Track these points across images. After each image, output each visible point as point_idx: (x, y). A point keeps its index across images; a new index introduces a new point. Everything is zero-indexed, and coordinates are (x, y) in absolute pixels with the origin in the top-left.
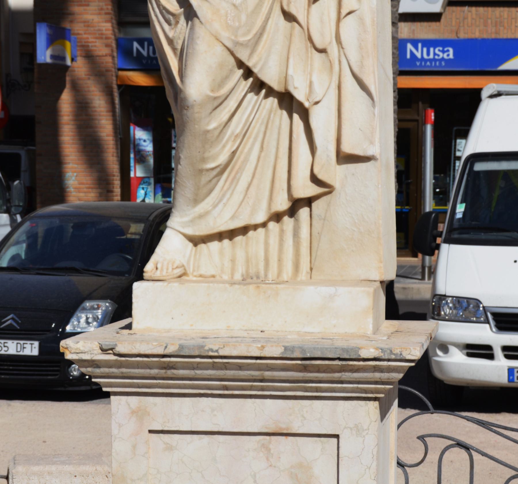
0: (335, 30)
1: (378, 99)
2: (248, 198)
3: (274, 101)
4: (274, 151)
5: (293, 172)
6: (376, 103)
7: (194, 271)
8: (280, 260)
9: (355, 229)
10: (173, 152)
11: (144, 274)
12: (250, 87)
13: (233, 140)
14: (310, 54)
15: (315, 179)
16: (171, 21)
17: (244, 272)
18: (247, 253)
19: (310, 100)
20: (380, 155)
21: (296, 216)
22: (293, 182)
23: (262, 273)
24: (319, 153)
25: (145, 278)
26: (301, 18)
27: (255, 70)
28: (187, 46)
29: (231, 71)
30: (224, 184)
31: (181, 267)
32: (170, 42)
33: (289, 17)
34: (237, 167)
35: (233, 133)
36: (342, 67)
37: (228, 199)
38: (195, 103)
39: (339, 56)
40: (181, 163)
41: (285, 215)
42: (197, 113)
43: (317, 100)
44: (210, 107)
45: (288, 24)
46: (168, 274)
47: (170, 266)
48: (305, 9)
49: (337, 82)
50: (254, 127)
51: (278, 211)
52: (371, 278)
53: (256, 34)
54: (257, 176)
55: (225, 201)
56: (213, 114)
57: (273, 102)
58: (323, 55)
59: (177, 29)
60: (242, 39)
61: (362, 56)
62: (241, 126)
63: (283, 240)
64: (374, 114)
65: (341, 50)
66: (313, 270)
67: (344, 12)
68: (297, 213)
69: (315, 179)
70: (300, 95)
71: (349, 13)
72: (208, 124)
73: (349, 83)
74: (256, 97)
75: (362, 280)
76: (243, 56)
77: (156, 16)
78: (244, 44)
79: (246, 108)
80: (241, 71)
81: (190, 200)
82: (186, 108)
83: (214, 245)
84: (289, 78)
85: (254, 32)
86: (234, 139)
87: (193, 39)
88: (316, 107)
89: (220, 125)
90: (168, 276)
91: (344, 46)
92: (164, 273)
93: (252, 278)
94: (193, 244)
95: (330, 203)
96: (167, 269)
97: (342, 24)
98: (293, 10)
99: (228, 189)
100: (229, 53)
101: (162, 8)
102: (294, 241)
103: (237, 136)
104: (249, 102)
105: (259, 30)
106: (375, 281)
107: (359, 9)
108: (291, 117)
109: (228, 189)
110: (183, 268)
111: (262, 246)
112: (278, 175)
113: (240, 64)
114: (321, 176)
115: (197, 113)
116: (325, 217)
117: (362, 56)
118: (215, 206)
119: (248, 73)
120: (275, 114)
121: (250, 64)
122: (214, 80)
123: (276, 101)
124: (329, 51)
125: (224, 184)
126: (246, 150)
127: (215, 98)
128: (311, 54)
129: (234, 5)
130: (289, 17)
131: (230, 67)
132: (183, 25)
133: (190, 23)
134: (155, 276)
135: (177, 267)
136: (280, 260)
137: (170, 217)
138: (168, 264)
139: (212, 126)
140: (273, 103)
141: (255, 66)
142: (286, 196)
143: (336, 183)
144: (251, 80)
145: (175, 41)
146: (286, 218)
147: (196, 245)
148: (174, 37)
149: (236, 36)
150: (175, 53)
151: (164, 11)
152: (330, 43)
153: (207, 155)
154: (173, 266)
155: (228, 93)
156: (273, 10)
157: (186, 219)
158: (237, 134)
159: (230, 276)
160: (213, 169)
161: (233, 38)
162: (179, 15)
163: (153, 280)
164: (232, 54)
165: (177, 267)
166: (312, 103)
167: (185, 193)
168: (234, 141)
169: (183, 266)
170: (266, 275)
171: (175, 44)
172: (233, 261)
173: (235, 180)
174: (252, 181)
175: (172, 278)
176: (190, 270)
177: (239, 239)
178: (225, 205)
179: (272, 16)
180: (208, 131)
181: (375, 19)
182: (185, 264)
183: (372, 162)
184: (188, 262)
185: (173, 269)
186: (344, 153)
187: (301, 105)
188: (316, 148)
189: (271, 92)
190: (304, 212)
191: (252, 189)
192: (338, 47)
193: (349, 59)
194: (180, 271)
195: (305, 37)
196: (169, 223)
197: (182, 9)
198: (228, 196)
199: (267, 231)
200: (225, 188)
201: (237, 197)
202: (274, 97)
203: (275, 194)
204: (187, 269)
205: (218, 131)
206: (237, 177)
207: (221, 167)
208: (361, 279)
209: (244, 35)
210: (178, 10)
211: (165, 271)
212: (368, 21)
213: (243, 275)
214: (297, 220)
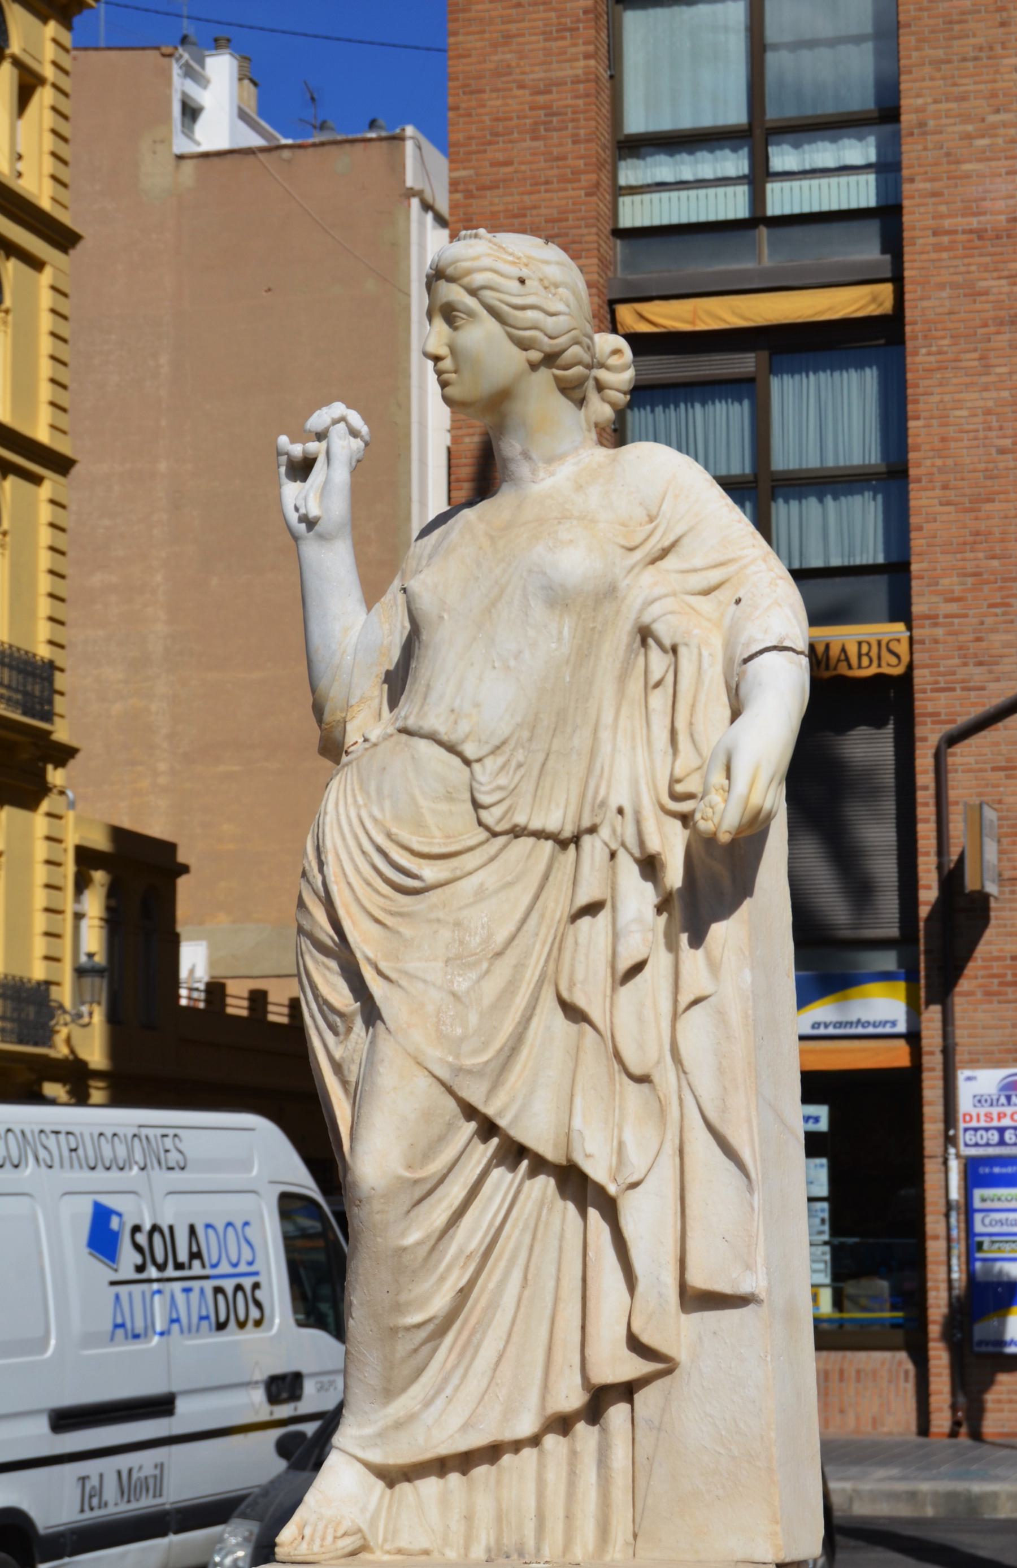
0: (669, 1035)
1: (760, 1176)
2: (497, 1384)
3: (548, 1182)
4: (551, 1284)
5: (589, 1329)
6: (754, 1183)
7: (385, 1540)
8: (569, 1517)
9: (722, 1451)
10: (823, 1191)
11: (277, 1550)
12: (494, 1155)
13: (462, 1264)
14: (618, 1086)
15: (636, 1345)
16: (337, 1027)
17: (492, 1543)
18: (498, 1501)
19: (620, 1181)
20: (769, 1291)
21: (602, 1421)
22: (588, 1351)
23: (531, 1543)
24: (641, 1287)
25: (278, 1557)
26: (595, 1014)
27: (502, 1123)
28: (364, 1078)
29: (450, 1126)
30: (448, 1357)
31: (354, 1534)
32: (338, 1068)
33: (573, 1012)
34: (473, 1321)
35: (461, 1251)
36: (686, 1111)
37: (457, 1388)
38: (373, 1192)
39: (680, 1087)
40: (354, 1315)
41: (579, 1421)
42: (378, 1212)
43: (634, 1179)
44: (405, 1200)
45: (572, 1028)
46: (323, 1550)
47: (330, 1531)
48: (605, 996)
49: (677, 1142)
50: (509, 1237)
51: (560, 1412)
52: (757, 1559)
53: (501, 1049)
54: (515, 1338)
55: (449, 1391)
56: (413, 1214)
57: (545, 1184)
58: (645, 1087)
59: (348, 1044)
60: (468, 1062)
61: (725, 1089)
62: (480, 1235)
63: (575, 1473)
64: (753, 1209)
65: (682, 1075)
66: (638, 1539)
67: (684, 1000)
68: (605, 1415)
69: (636, 1345)
70: (597, 1171)
71: (696, 1002)
72: (403, 1235)
73: (701, 1143)
74: (510, 1176)
75: (737, 1562)
76: (475, 1096)
77: (312, 1017)
78: (475, 1070)
79: (490, 1199)
80: (472, 1126)
81: (375, 1390)
82: (358, 1202)
83: (430, 1486)
84: (575, 1135)
85: (496, 1045)
86: (465, 1264)
87: (372, 1063)
88: (632, 1193)
89: (428, 1236)
90: (323, 1553)
91: (687, 1070)
92: (316, 1548)
93: (508, 1557)
94: (385, 1482)
95: (669, 1393)
96: (323, 1539)
97: (680, 1025)
98: (580, 1001)
99: (455, 1367)
100: (443, 1089)
101: (321, 1002)
102: (599, 1475)
103: (469, 1257)
104: (497, 1186)
105: (508, 1040)
106: (764, 1563)
107: (716, 992)
108: (584, 1214)
109: (455, 1367)
110: (359, 1535)
111: (531, 1486)
112: (559, 1334)
113: (470, 1112)
114: (647, 1338)
115: (378, 1212)
116: (661, 1423)
117: (725, 1089)
118: (428, 1403)
119: (488, 1129)
120: (550, 1210)
121: (490, 1110)
123: (552, 1182)
124: (656, 1078)
125: (448, 1357)
126: (491, 1286)
127: (416, 1182)
128: (621, 1085)
129: (454, 994)
130: (573, 1012)
131: (447, 1118)
132: (359, 1035)
133: (371, 1029)
134: (296, 1552)
135: (345, 1534)
136: (569, 1517)
137: (340, 1427)
138: (326, 1527)
139: (412, 1238)
140: (546, 1187)
141: (500, 1113)
142: (578, 1379)
143: (681, 1353)
144: (495, 1141)
145: (345, 1067)
146: (581, 1427)
147: (391, 1484)
148: (342, 1058)
149: (457, 1056)
150: (346, 1091)
151: (325, 1008)
152: (658, 1062)
153: (403, 1297)
154: (335, 1531)
155: (445, 1171)
156: (541, 1000)
157: (369, 1430)
158: (471, 1253)
159: (462, 1551)
160: (419, 1326)
161: (450, 1059)
162: (353, 1014)
163: (293, 1563)
164: (450, 1091)
165: (345, 1534)
166: (624, 1186)
167: (365, 1377)
168: (465, 1266)
169: (360, 1530)
170: (538, 1549)
171: (346, 1072)
172: (469, 1518)
173: (470, 1348)
174: (505, 1347)
175: (332, 1559)
176: (377, 1538)
177: (481, 1471)
178: (450, 1400)
179: (538, 1011)
180: (405, 1249)
181: (750, 1012)
182: (364, 1527)
183: (752, 1306)
184: (373, 1522)
185: (335, 1538)
186: (693, 1287)
187: (601, 1190)
188: (636, 1278)
189: (539, 1165)
190: (617, 1413)
191: (505, 1368)
192: (677, 1070)
193: (697, 1094)
194: (353, 1543)
195: (607, 1051)
196: (338, 1439)
197: (358, 1004)
198: (455, 1380)
199: (542, 1454)
200: (449, 1365)
201: (475, 1383)
202: (549, 1175)
203: (553, 1377)
204: (369, 1537)
205: (426, 1248)
206: (475, 1341)
207: (437, 1322)
208: (735, 1559)
209: (476, 1052)
210: (351, 1005)
211: (318, 1542)
212: (735, 1017)
213: (489, 1550)
214: (604, 1431)
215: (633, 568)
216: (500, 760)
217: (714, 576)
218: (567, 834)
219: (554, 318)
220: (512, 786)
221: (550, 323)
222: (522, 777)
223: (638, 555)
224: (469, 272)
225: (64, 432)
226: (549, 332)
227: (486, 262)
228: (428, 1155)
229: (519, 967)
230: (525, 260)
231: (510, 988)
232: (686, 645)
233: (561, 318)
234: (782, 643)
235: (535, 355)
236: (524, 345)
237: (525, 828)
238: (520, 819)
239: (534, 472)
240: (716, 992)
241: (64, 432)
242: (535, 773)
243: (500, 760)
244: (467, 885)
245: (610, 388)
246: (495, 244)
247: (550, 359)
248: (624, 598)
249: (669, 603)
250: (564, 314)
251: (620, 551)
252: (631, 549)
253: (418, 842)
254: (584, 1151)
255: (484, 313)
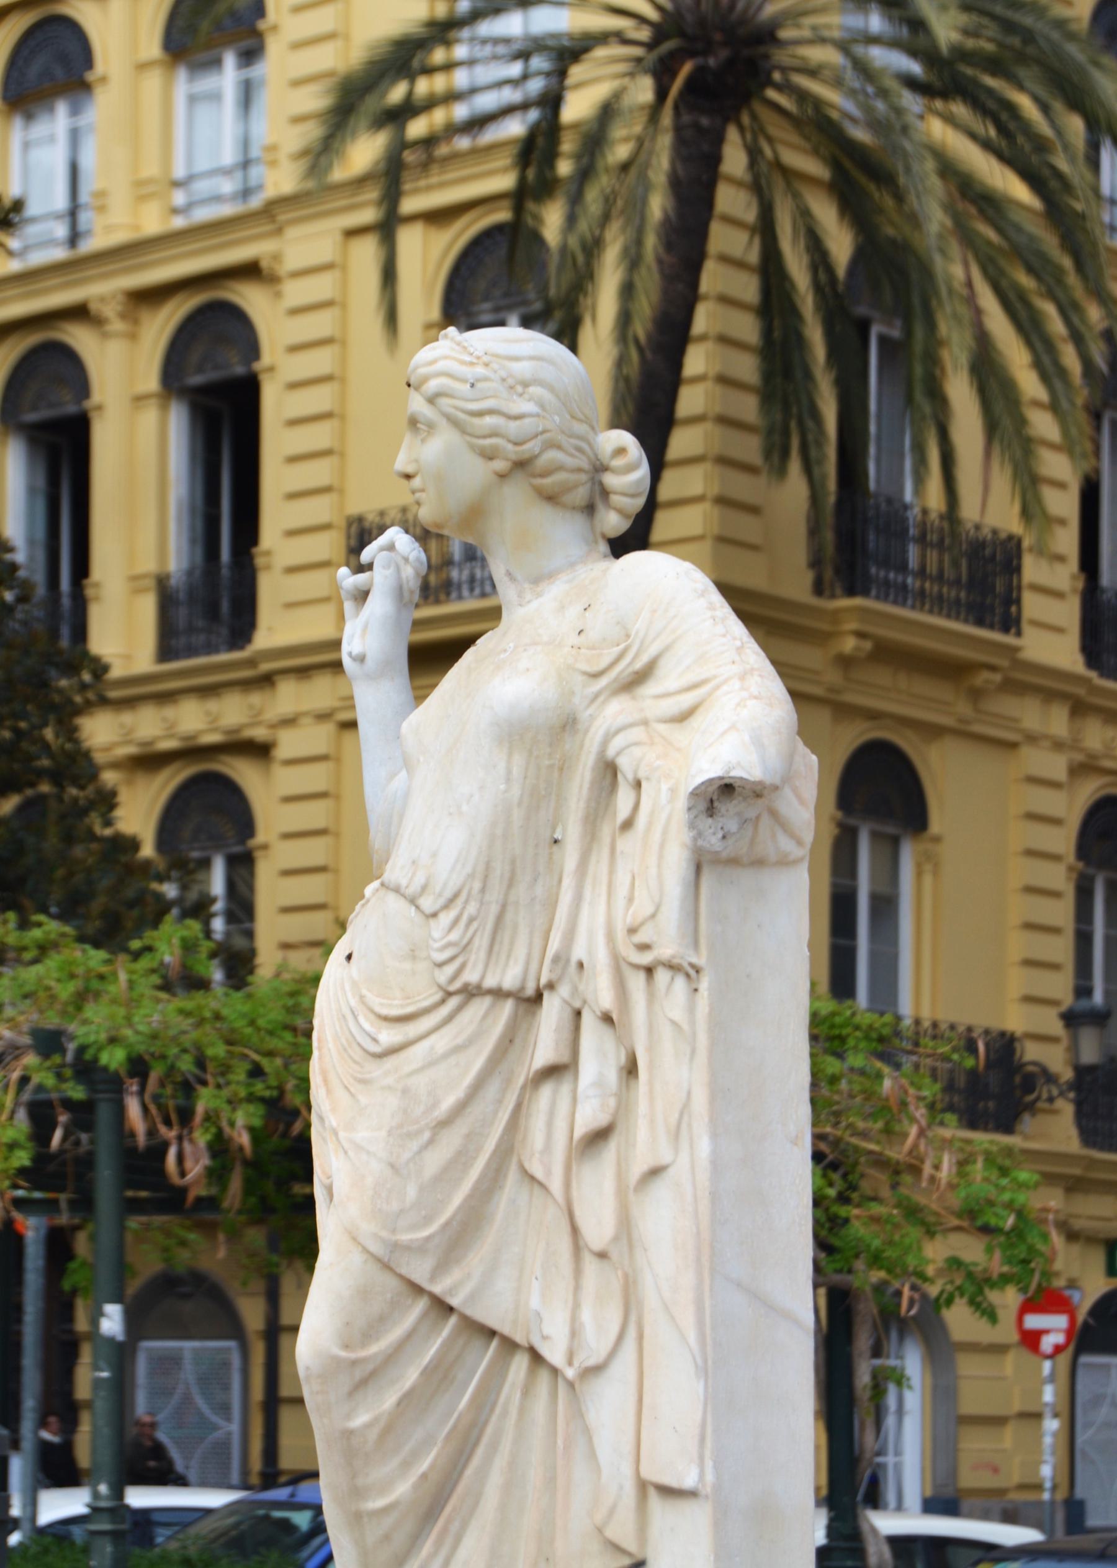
43: (591, 1362)
60: (405, 1237)
72: (348, 1416)
122: (348, 1323)
127: (354, 1363)
139: (360, 1420)
149: (394, 1231)
209: (414, 1227)
215: (596, 696)
216: (452, 914)
217: (686, 700)
218: (530, 991)
219: (518, 423)
220: (465, 941)
221: (513, 427)
222: (476, 932)
223: (604, 681)
224: (425, 379)
225: (753, 547)
226: (512, 438)
227: (441, 366)
228: (368, 1335)
229: (473, 1139)
230: (485, 359)
231: (461, 1159)
232: (648, 779)
233: (527, 421)
234: (729, 772)
235: (500, 465)
236: (488, 455)
237: (479, 987)
238: (471, 976)
239: (520, 595)
240: (674, 1162)
241: (753, 547)
242: (489, 926)
243: (452, 914)
244: (419, 1051)
245: (615, 493)
246: (459, 344)
247: (521, 465)
248: (587, 731)
249: (637, 734)
250: (530, 415)
251: (580, 678)
252: (596, 675)
253: (382, 1004)
254: (541, 1331)
255: (443, 423)
